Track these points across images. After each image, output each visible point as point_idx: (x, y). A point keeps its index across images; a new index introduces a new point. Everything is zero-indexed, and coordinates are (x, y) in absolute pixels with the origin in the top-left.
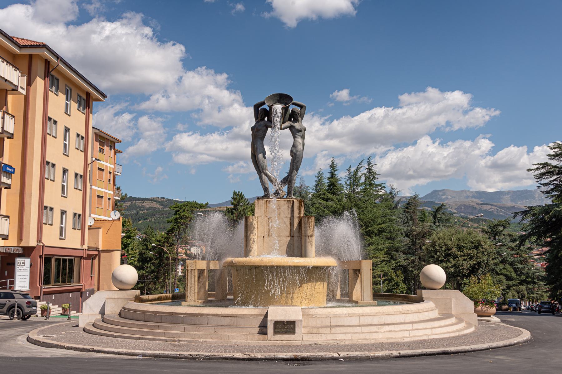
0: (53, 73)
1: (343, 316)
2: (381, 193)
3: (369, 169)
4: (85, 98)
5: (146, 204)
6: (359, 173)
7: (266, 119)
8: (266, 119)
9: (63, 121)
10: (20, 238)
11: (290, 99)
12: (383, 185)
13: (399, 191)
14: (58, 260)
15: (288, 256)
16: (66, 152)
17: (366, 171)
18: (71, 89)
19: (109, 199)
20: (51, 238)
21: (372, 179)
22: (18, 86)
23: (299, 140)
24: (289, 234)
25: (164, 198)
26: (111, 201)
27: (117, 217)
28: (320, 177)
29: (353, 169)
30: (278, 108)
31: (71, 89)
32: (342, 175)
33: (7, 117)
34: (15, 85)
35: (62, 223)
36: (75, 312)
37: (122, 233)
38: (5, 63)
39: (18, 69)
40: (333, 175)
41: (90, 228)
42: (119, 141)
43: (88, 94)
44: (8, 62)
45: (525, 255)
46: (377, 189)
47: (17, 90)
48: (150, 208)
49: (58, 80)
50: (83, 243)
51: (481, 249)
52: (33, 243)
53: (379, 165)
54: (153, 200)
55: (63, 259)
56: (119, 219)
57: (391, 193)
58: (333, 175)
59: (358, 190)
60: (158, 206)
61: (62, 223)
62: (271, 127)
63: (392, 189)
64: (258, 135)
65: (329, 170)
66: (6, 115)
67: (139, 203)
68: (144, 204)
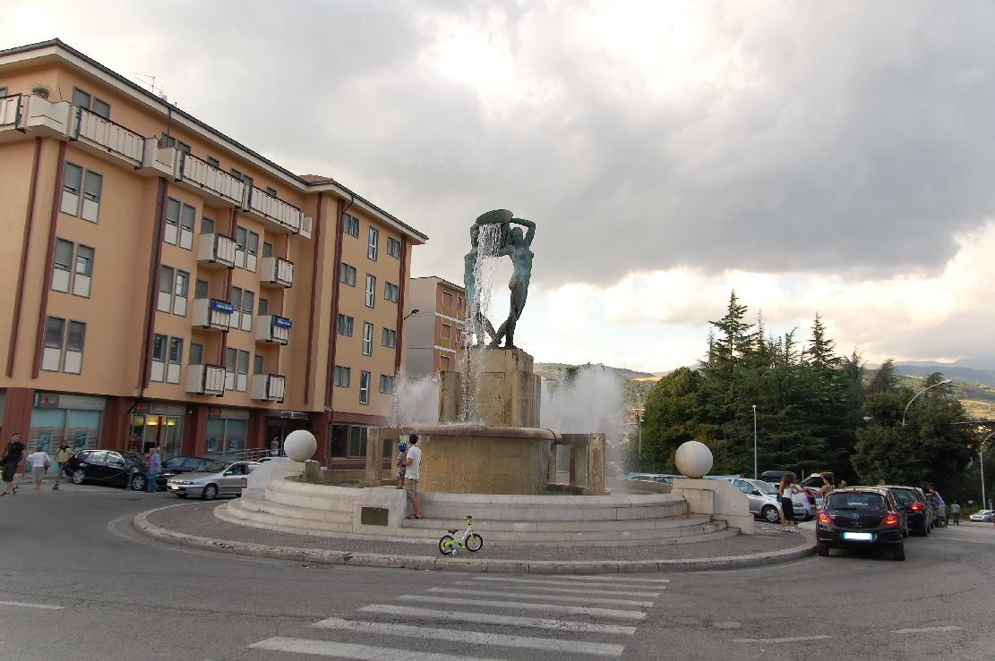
10: (306, 402)
52: (318, 406)
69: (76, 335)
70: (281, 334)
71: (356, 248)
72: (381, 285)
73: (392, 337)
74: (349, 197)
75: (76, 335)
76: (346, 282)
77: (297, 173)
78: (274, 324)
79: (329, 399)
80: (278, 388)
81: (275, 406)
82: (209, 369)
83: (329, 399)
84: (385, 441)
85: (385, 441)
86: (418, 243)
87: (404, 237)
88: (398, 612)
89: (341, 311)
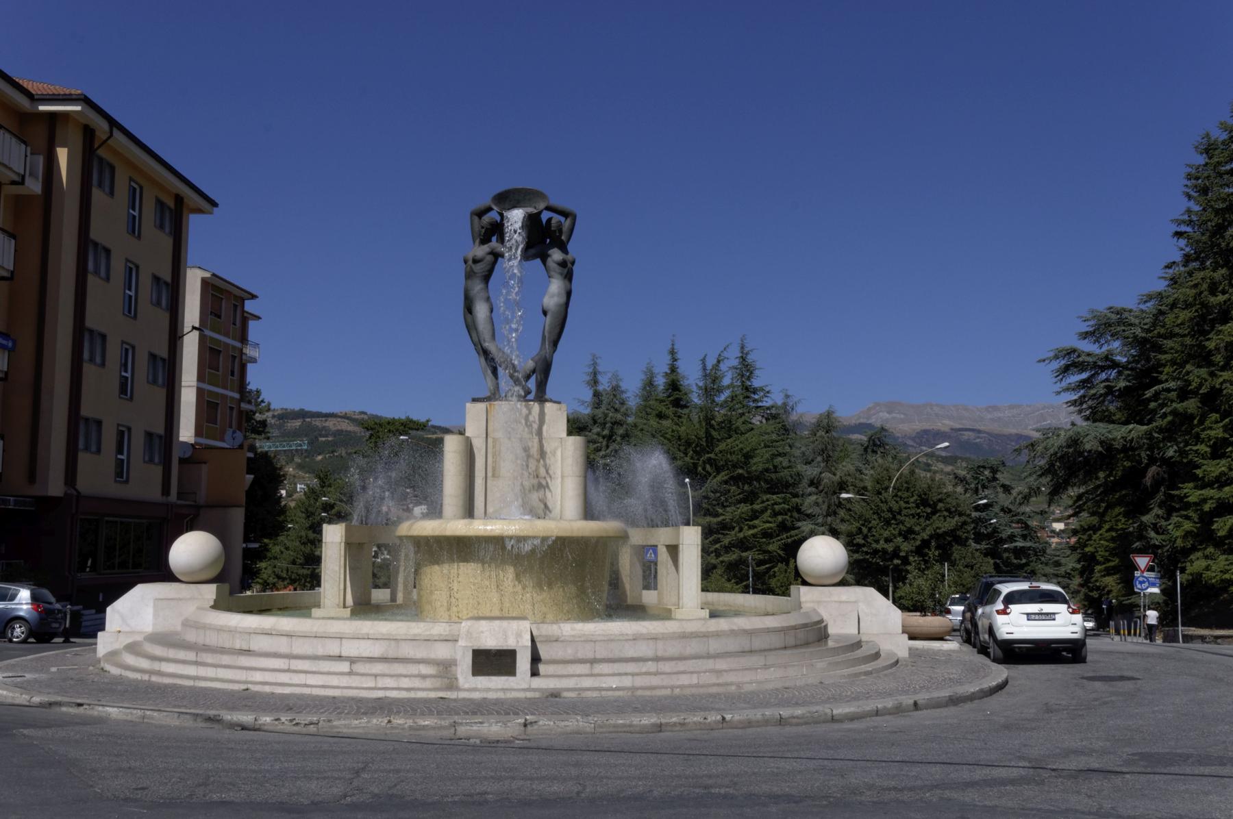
0: (101, 152)
2: (764, 404)
3: (743, 359)
5: (331, 424)
6: (723, 367)
9: (121, 246)
10: (32, 477)
13: (799, 401)
15: (319, 586)
16: (130, 312)
18: (141, 188)
19: (231, 408)
20: (96, 476)
21: (749, 378)
22: (23, 177)
24: (250, 367)
25: (365, 413)
28: (650, 384)
29: (710, 363)
30: (516, 217)
31: (141, 188)
32: (692, 378)
35: (120, 451)
39: (25, 143)
40: (673, 369)
41: (182, 461)
42: (253, 297)
43: (179, 199)
45: (1034, 523)
46: (756, 397)
48: (340, 432)
49: (112, 168)
50: (166, 490)
51: (1191, 514)
52: (55, 487)
54: (345, 417)
57: (785, 405)
58: (673, 369)
59: (722, 398)
60: (351, 427)
61: (120, 451)
63: (787, 396)
65: (667, 359)
67: (318, 422)
68: (327, 424)
72: (146, 281)
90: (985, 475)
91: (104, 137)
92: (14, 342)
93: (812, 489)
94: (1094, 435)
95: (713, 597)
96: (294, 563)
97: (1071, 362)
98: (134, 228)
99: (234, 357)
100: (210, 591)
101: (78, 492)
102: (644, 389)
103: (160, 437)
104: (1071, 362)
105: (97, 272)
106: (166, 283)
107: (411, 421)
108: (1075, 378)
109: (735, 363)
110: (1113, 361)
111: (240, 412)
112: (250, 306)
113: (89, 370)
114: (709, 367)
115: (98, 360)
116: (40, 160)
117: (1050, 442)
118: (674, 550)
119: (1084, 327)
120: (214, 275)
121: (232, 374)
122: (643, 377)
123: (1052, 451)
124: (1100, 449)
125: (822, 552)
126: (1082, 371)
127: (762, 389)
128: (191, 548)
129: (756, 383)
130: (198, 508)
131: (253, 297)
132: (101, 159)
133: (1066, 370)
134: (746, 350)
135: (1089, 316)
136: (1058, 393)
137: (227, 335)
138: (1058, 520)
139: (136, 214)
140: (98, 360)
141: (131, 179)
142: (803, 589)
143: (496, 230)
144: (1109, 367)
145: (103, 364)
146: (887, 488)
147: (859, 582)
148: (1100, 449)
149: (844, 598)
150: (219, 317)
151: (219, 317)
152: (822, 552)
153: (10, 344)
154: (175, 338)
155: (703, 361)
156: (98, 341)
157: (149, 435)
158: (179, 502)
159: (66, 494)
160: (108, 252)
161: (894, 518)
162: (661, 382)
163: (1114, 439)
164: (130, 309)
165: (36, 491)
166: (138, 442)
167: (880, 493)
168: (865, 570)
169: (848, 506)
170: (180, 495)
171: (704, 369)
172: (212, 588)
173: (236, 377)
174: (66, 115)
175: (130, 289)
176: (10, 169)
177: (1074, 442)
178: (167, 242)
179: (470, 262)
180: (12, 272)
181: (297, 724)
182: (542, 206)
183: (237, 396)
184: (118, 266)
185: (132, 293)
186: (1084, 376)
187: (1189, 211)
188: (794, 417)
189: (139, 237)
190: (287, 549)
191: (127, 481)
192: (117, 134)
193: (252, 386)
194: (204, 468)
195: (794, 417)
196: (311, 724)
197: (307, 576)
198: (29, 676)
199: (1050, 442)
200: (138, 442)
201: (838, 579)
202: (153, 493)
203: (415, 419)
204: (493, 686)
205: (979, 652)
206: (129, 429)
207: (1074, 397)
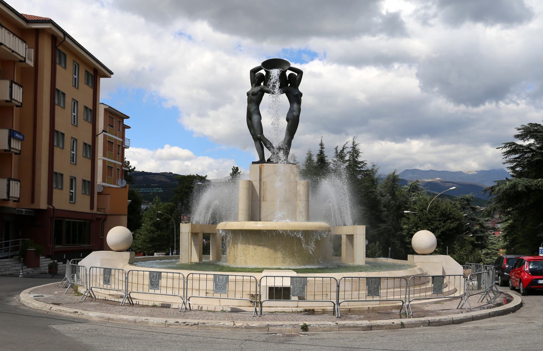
1: (56, 318)
2: (364, 169)
4: (92, 74)
6: (345, 151)
7: (262, 84)
8: (262, 84)
9: (70, 93)
10: (33, 201)
11: (288, 63)
12: (365, 162)
14: (69, 223)
16: (74, 123)
17: (350, 150)
18: (78, 65)
19: (118, 169)
20: (61, 202)
21: (356, 157)
22: (25, 58)
23: (295, 106)
26: (120, 171)
27: (124, 185)
28: (309, 159)
30: (275, 73)
31: (78, 65)
33: (15, 87)
34: (22, 57)
35: (71, 189)
36: (62, 263)
37: (129, 199)
38: (11, 35)
39: (25, 42)
40: (322, 152)
41: (99, 194)
42: (128, 117)
44: (14, 34)
46: (360, 166)
47: (25, 61)
49: (65, 55)
50: (92, 207)
52: (43, 205)
53: (326, 182)
55: (79, 222)
56: (125, 187)
57: (373, 169)
60: (165, 180)
61: (71, 189)
62: (268, 92)
64: (255, 100)
66: (14, 85)
68: (154, 178)
69: (107, 281)
70: (16, 145)
71: (65, 77)
72: (81, 109)
73: (88, 149)
74: (62, 35)
75: (107, 281)
76: (59, 105)
77: (20, 12)
78: (11, 135)
79: (50, 200)
80: (15, 190)
81: (11, 204)
82: (11, 182)
83: (50, 200)
84: (270, 288)
85: (270, 288)
86: (105, 76)
87: (96, 70)
88: (39, 306)
89: (57, 128)
90: (467, 203)
91: (61, 41)
92: (23, 136)
93: (385, 209)
94: (523, 182)
95: (370, 260)
96: (144, 241)
97: (514, 149)
98: (76, 85)
99: (119, 146)
100: (127, 255)
101: (54, 208)
102: (307, 162)
103: (89, 182)
104: (514, 149)
105: (59, 105)
106: (90, 110)
107: (198, 176)
108: (513, 156)
109: (350, 150)
110: (531, 149)
111: (122, 170)
112: (126, 122)
113: (57, 151)
114: (339, 151)
115: (61, 146)
116: (32, 51)
117: (501, 186)
118: (351, 237)
119: (518, 133)
120: (110, 107)
121: (118, 154)
122: (307, 156)
123: (502, 191)
124: (525, 190)
125: (424, 238)
126: (516, 153)
127: (362, 162)
128: (117, 234)
129: (360, 159)
130: (106, 215)
131: (128, 117)
132: (60, 51)
133: (508, 153)
134: (355, 144)
135: (520, 127)
136: (504, 163)
137: (116, 135)
138: (405, 229)
139: (76, 77)
140: (61, 146)
141: (74, 61)
142: (415, 256)
143: (266, 79)
144: (529, 152)
145: (63, 148)
146: (425, 209)
147: (443, 253)
148: (525, 190)
149: (435, 260)
150: (112, 127)
151: (112, 127)
152: (424, 238)
153: (22, 137)
154: (94, 136)
155: (336, 148)
156: (61, 137)
157: (84, 181)
158: (98, 213)
159: (48, 208)
160: (64, 94)
161: (429, 222)
162: (315, 159)
163: (532, 186)
164: (75, 122)
165: (35, 206)
166: (79, 184)
167: (422, 211)
168: (444, 246)
169: (407, 216)
170: (98, 209)
171: (337, 152)
172: (128, 254)
173: (120, 155)
174: (43, 30)
175: (74, 113)
176: (19, 55)
177: (514, 186)
178: (91, 91)
179: (250, 95)
180: (21, 103)
181: (187, 325)
182: (287, 67)
183: (121, 164)
184: (68, 101)
185: (75, 114)
186: (517, 156)
187: (130, 167)
188: (376, 177)
189: (78, 88)
190: (141, 235)
191: (75, 203)
192: (67, 39)
193: (127, 160)
194: (109, 197)
195: (376, 177)
196: (195, 325)
197: (150, 247)
198: (45, 296)
199: (501, 186)
200: (79, 184)
201: (432, 251)
202: (86, 209)
203: (200, 175)
204: (280, 305)
205: (511, 289)
206: (75, 178)
207: (512, 165)
